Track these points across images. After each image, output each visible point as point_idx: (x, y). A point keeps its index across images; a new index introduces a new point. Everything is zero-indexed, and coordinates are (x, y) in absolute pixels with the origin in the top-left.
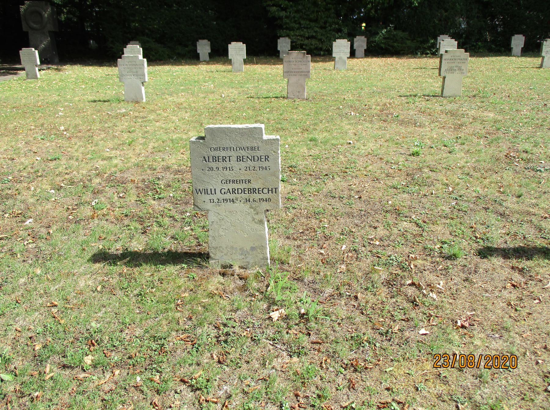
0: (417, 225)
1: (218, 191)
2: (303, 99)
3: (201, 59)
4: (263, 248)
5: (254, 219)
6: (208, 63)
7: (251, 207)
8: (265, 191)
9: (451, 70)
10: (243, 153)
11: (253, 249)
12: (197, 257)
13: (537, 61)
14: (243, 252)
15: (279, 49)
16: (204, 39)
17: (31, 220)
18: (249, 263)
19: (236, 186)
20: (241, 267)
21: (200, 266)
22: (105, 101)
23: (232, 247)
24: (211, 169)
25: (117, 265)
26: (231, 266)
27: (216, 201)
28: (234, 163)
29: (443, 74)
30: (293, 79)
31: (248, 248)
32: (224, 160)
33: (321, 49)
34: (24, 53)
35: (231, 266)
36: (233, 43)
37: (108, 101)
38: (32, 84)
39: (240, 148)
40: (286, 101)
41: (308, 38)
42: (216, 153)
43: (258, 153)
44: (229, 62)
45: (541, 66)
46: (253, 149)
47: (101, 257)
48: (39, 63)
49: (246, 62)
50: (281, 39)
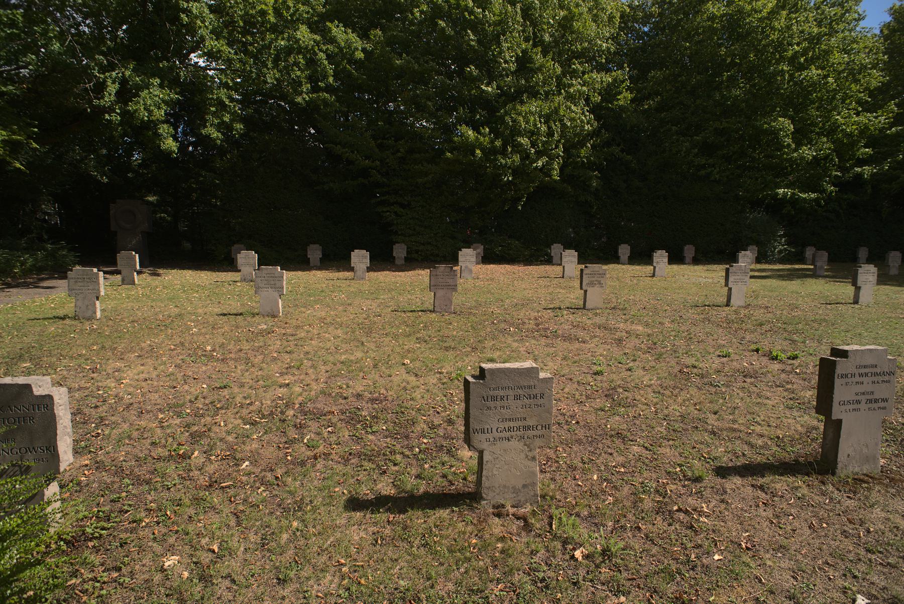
0: (646, 448)
1: (494, 430)
2: (451, 313)
3: (311, 264)
4: (534, 484)
5: (527, 456)
6: (319, 268)
7: (525, 445)
8: (539, 427)
9: (591, 284)
10: (520, 392)
11: (524, 486)
12: (465, 498)
13: (650, 268)
14: (516, 491)
15: (394, 254)
16: (315, 243)
17: (247, 463)
18: (520, 501)
19: (512, 424)
20: (513, 506)
21: (472, 509)
22: (236, 315)
23: (505, 486)
24: (489, 408)
25: (379, 512)
26: (503, 506)
27: (492, 440)
28: (511, 401)
29: (584, 287)
30: (440, 293)
31: (520, 486)
32: (502, 399)
33: (437, 255)
34: (121, 256)
35: (503, 506)
36: (356, 251)
37: (241, 314)
38: (124, 291)
39: (519, 388)
40: (434, 315)
41: (423, 244)
42: (496, 393)
43: (534, 392)
44: (352, 269)
45: (653, 276)
46: (529, 387)
47: (354, 504)
48: (138, 267)
49: (369, 269)
50: (397, 245)
